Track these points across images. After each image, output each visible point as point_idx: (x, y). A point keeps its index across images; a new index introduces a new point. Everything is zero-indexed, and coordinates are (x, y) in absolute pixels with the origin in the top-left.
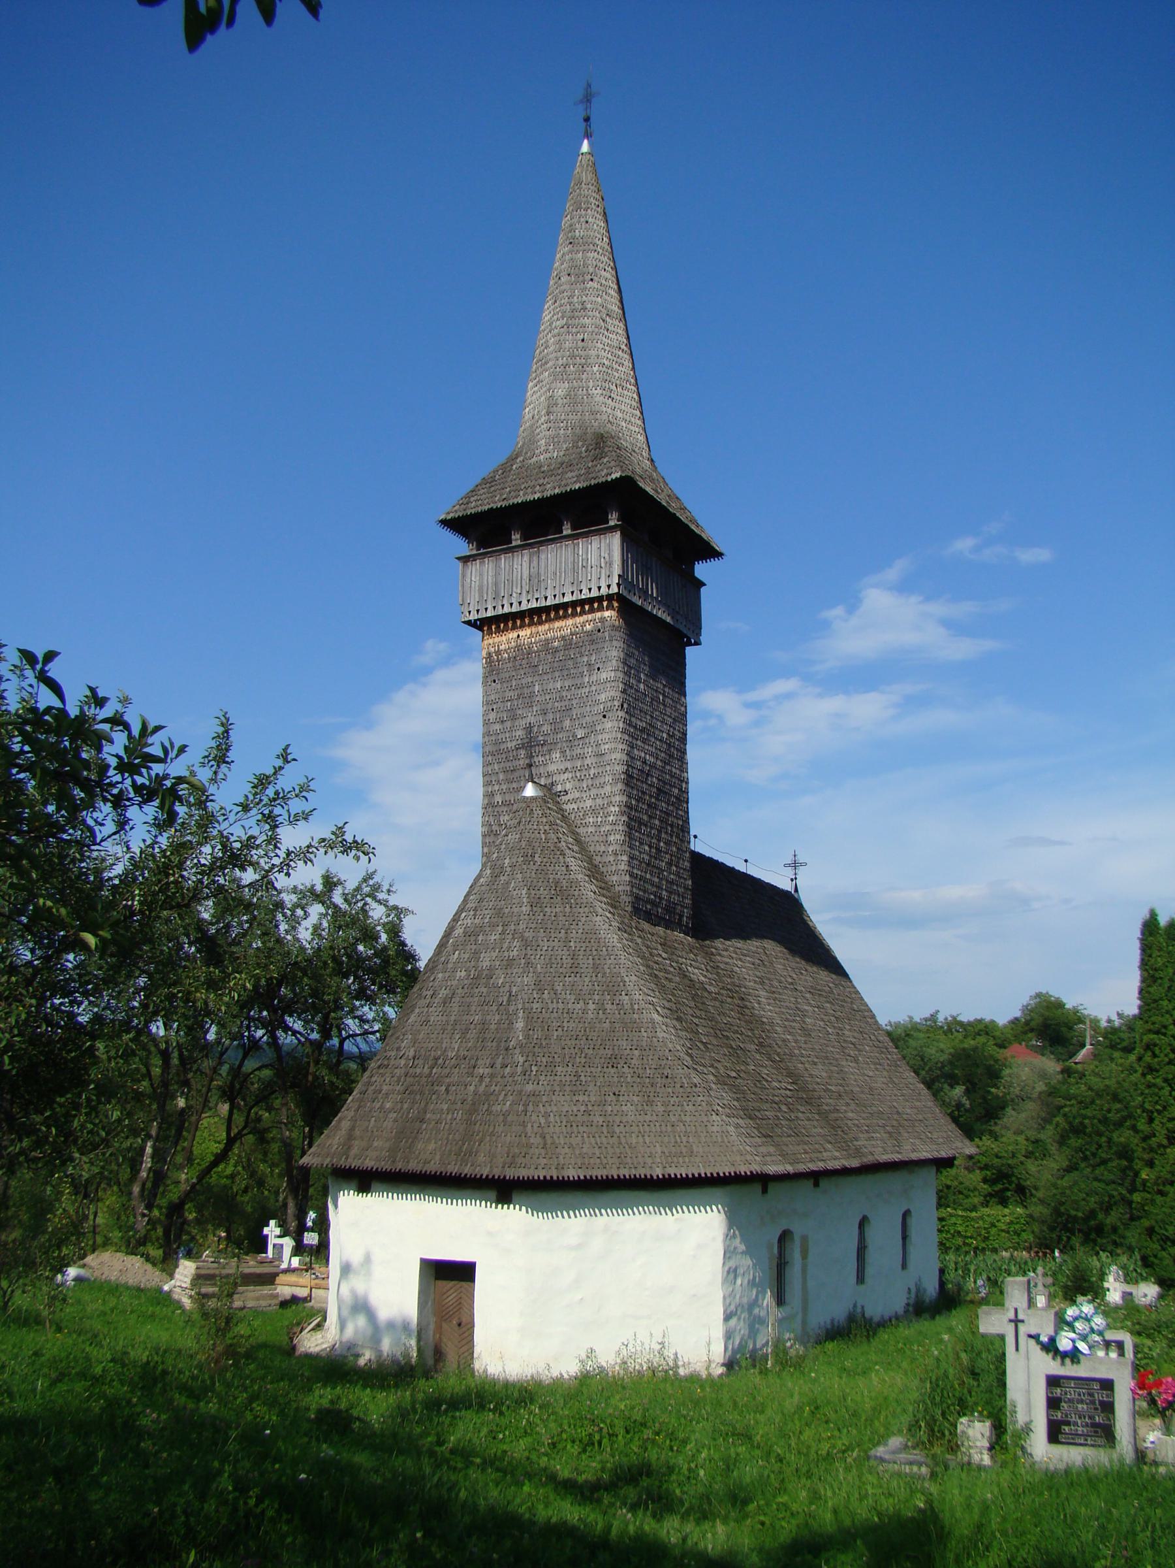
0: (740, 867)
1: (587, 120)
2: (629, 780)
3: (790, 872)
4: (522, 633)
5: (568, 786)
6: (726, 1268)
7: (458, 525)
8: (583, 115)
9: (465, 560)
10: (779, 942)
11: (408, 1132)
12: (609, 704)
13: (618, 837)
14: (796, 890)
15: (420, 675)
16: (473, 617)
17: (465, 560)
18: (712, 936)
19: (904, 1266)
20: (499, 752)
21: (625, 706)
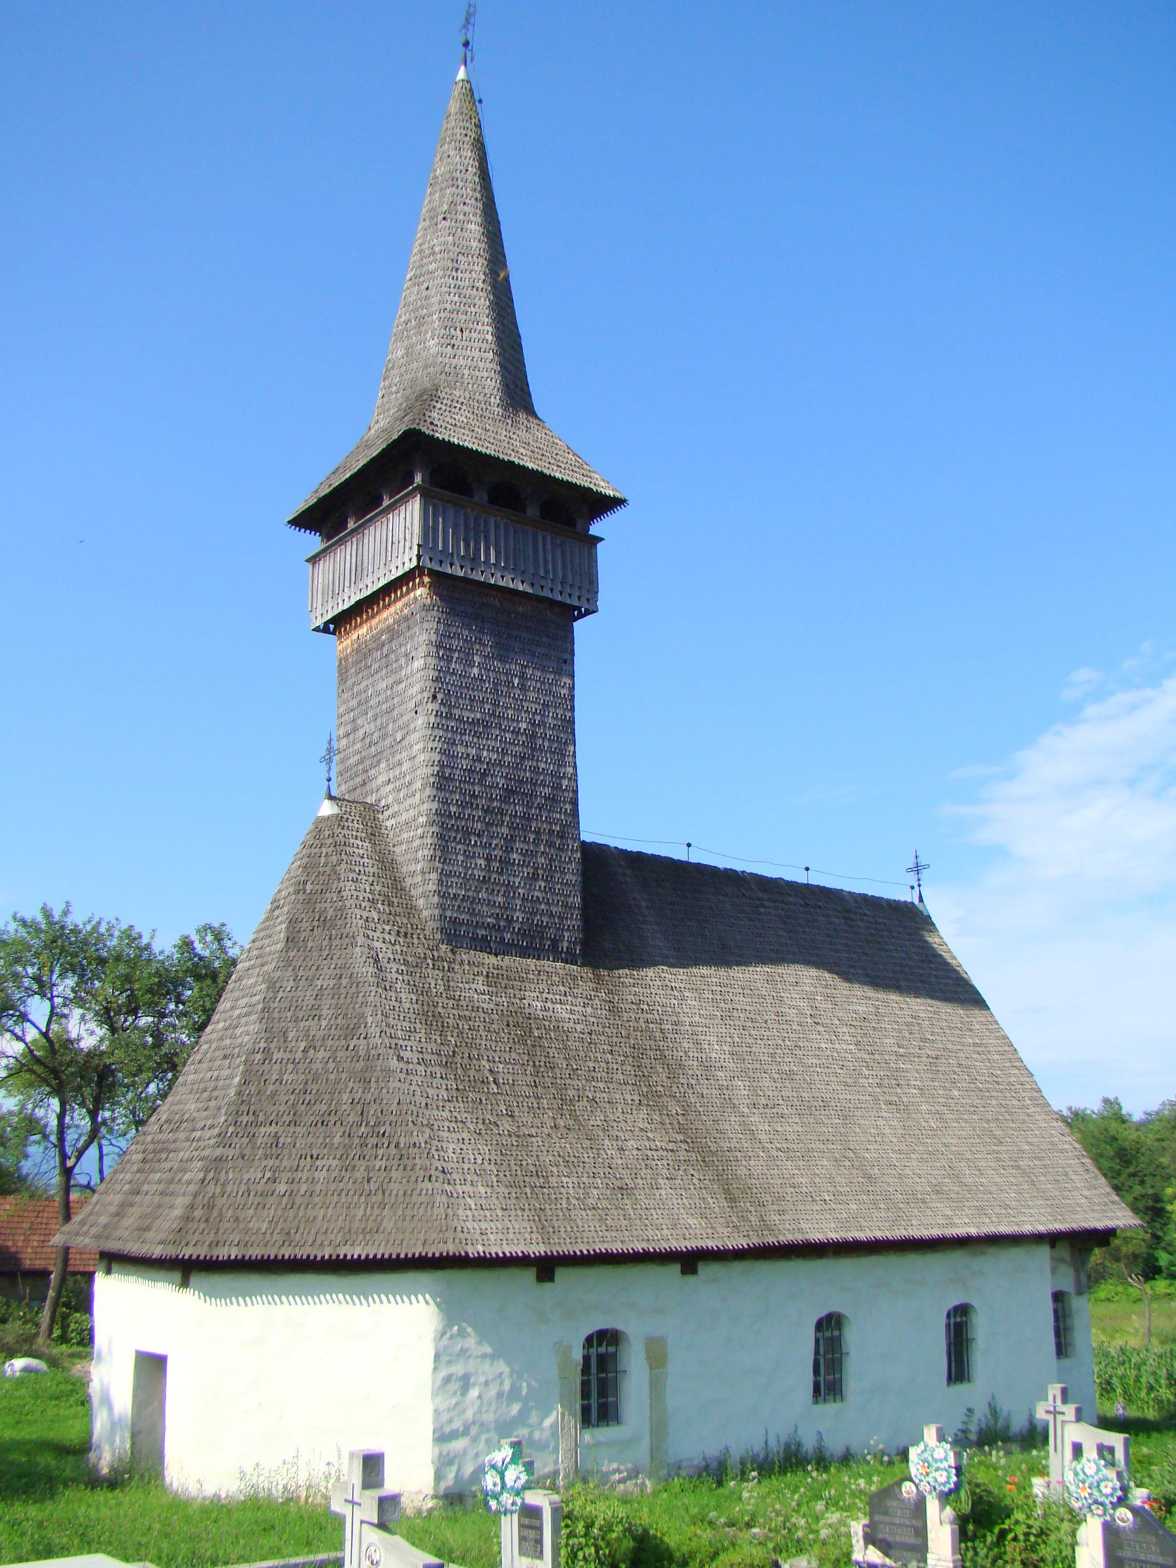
0: (800, 878)
1: (466, 44)
2: (443, 782)
3: (912, 879)
4: (360, 632)
5: (390, 799)
6: (442, 1374)
7: (306, 520)
8: (463, 40)
9: (314, 560)
10: (948, 964)
11: (205, 1208)
12: (419, 697)
13: (426, 852)
14: (921, 900)
15: (1071, 714)
16: (320, 622)
17: (314, 560)
18: (637, 958)
19: (1062, 1348)
20: (347, 769)
21: (440, 696)
